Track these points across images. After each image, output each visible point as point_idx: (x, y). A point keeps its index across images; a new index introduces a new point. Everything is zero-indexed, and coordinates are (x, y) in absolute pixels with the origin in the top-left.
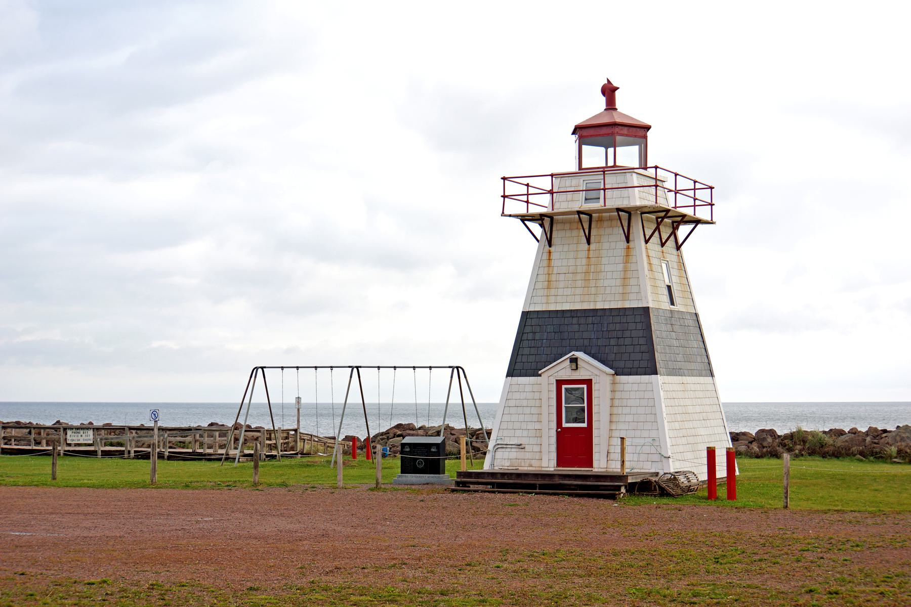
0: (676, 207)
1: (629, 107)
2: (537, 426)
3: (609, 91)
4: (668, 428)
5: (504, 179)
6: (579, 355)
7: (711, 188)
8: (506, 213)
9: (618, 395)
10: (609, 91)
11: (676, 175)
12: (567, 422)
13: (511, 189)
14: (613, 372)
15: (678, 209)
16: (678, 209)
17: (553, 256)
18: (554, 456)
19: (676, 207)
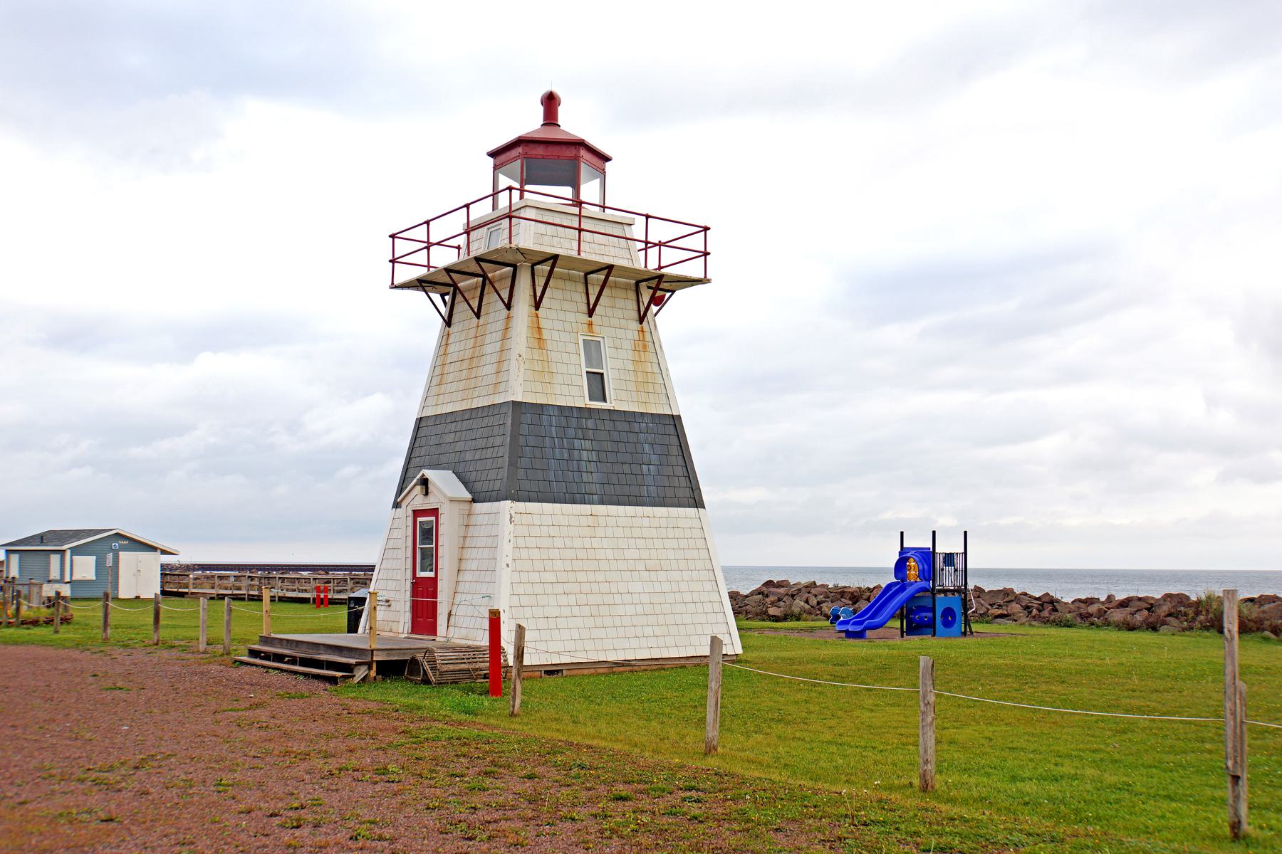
0: (660, 268)
1: (571, 123)
2: (68, 552)
3: (550, 101)
4: (566, 588)
5: (393, 236)
6: (428, 473)
7: (706, 229)
8: (396, 283)
9: (471, 531)
10: (550, 101)
11: (648, 217)
12: (422, 570)
13: (402, 247)
14: (469, 496)
15: (663, 271)
16: (663, 271)
17: (452, 339)
18: (408, 617)
19: (660, 268)
